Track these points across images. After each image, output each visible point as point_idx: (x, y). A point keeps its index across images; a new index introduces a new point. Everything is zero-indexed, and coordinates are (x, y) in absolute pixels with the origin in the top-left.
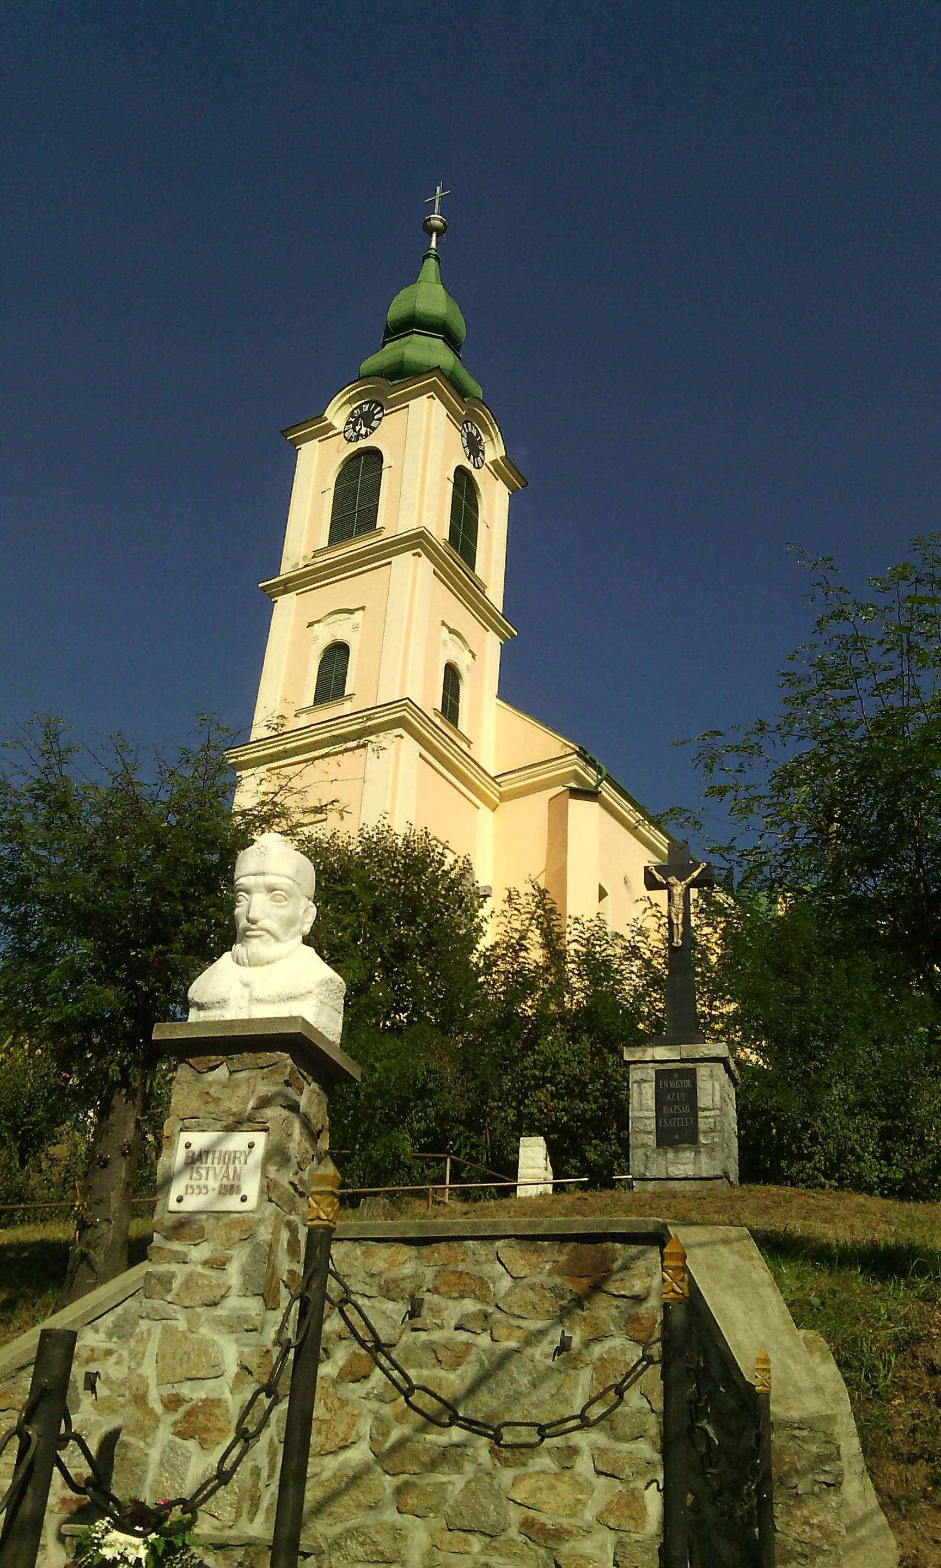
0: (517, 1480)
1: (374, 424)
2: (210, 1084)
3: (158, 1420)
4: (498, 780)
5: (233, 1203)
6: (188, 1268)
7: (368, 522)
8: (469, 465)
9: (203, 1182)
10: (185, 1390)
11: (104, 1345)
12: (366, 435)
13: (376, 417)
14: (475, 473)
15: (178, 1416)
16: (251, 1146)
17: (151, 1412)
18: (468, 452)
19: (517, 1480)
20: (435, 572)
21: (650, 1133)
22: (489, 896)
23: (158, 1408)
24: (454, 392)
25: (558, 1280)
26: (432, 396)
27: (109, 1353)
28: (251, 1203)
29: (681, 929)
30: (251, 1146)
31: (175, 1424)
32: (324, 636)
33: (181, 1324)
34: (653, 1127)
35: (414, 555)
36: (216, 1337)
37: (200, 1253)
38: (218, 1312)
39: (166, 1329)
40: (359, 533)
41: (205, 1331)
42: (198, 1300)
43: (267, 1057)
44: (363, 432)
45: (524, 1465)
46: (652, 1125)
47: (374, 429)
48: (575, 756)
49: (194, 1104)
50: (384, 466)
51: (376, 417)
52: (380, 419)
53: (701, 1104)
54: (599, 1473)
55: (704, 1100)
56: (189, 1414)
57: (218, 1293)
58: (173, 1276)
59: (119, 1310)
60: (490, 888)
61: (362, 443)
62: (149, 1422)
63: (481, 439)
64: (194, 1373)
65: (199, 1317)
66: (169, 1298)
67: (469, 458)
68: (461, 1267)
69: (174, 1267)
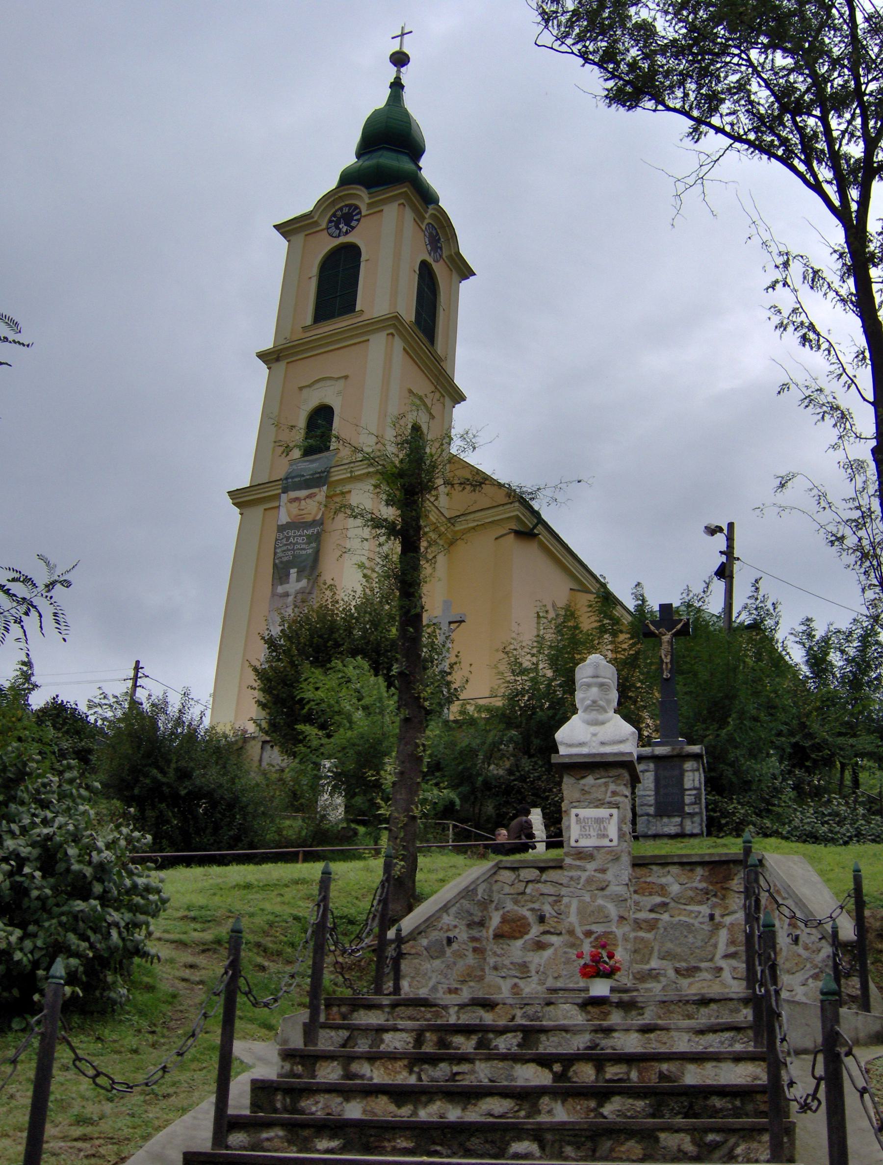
0: (690, 984)
1: (354, 224)
2: (584, 785)
3: (582, 941)
4: (452, 521)
5: (606, 842)
6: (587, 873)
7: (348, 306)
8: (430, 260)
9: (587, 833)
10: (594, 928)
11: (454, 923)
12: (347, 233)
13: (355, 218)
14: (435, 266)
15: (592, 939)
16: (611, 815)
17: (578, 938)
18: (429, 248)
19: (690, 984)
20: (404, 349)
21: (651, 806)
22: (464, 621)
23: (581, 936)
24: (418, 197)
25: (704, 885)
26: (403, 204)
27: (455, 927)
28: (615, 843)
29: (669, 666)
30: (611, 815)
31: (591, 943)
32: (313, 400)
33: (587, 898)
34: (653, 802)
35: (388, 334)
36: (606, 904)
37: (591, 866)
38: (606, 892)
39: (580, 901)
40: (340, 315)
41: (600, 902)
42: (594, 887)
43: (614, 772)
44: (344, 230)
45: (694, 977)
46: (651, 800)
47: (353, 228)
48: (517, 504)
49: (577, 795)
50: (362, 259)
51: (355, 218)
52: (358, 220)
53: (686, 787)
54: (734, 978)
55: (688, 784)
56: (596, 939)
57: (604, 884)
58: (579, 878)
59: (458, 905)
60: (465, 615)
61: (343, 240)
62: (578, 942)
63: (439, 239)
64: (598, 920)
65: (596, 895)
66: (579, 887)
67: (430, 254)
68: (648, 880)
69: (579, 873)
